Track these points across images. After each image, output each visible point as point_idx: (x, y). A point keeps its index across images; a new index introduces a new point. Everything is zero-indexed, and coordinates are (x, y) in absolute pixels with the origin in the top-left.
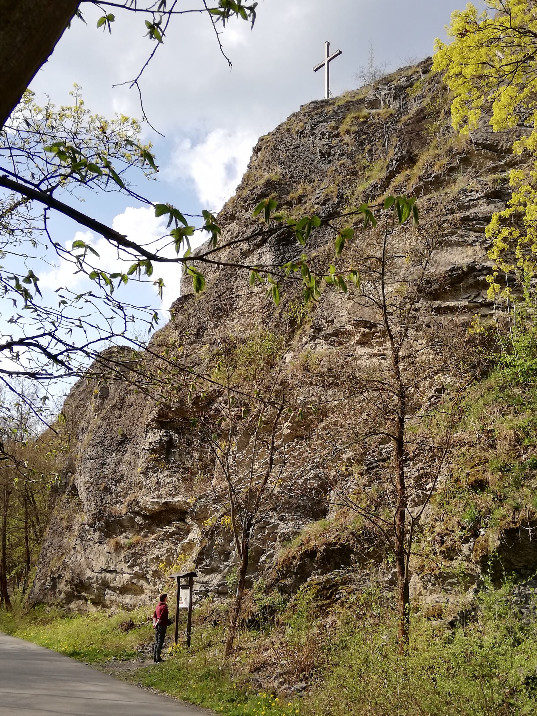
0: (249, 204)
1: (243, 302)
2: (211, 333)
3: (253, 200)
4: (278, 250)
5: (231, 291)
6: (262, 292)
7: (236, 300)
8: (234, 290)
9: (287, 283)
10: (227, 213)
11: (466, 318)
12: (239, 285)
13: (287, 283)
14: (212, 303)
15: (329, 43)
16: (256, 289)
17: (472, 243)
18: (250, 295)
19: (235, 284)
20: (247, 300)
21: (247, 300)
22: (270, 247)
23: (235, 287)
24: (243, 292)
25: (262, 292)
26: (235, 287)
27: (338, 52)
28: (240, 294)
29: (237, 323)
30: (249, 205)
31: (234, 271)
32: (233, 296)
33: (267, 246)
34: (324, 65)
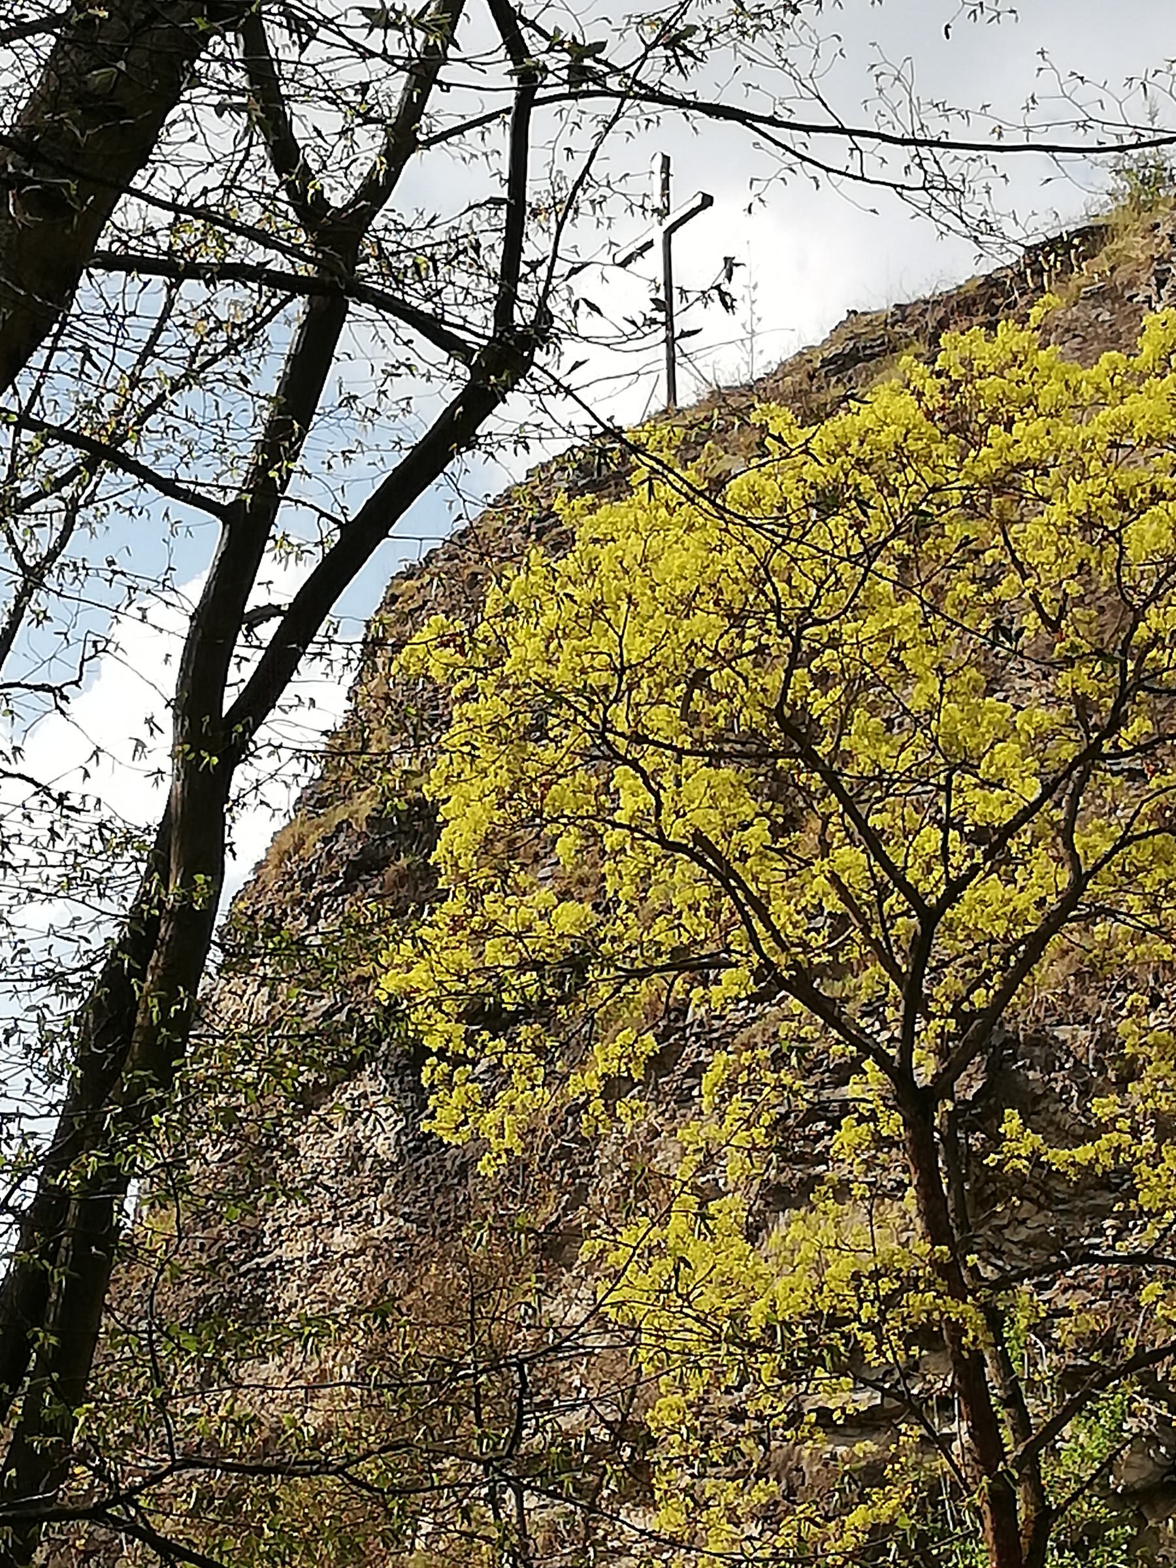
0: (322, 895)
1: (300, 1289)
2: (190, 1410)
3: (331, 879)
4: (411, 1090)
5: (255, 1246)
6: (362, 1252)
7: (274, 1279)
8: (266, 1241)
9: (443, 1224)
10: (255, 912)
11: (875, 1448)
12: (283, 1222)
13: (443, 1224)
14: (190, 1292)
15: (666, 160)
16: (342, 1239)
17: (893, 1189)
18: (322, 1260)
19: (269, 1215)
20: (312, 1280)
21: (312, 1280)
22: (386, 1077)
23: (268, 1227)
24: (295, 1249)
25: (362, 1252)
26: (268, 1227)
27: (698, 201)
28: (288, 1256)
29: (280, 1368)
30: (319, 898)
31: (265, 1165)
32: (264, 1262)
33: (374, 1073)
34: (649, 245)
